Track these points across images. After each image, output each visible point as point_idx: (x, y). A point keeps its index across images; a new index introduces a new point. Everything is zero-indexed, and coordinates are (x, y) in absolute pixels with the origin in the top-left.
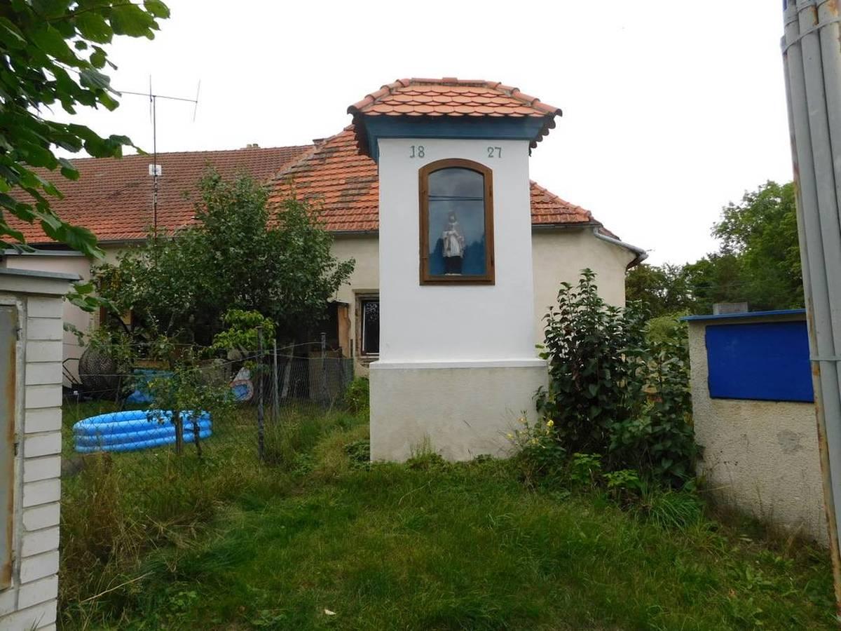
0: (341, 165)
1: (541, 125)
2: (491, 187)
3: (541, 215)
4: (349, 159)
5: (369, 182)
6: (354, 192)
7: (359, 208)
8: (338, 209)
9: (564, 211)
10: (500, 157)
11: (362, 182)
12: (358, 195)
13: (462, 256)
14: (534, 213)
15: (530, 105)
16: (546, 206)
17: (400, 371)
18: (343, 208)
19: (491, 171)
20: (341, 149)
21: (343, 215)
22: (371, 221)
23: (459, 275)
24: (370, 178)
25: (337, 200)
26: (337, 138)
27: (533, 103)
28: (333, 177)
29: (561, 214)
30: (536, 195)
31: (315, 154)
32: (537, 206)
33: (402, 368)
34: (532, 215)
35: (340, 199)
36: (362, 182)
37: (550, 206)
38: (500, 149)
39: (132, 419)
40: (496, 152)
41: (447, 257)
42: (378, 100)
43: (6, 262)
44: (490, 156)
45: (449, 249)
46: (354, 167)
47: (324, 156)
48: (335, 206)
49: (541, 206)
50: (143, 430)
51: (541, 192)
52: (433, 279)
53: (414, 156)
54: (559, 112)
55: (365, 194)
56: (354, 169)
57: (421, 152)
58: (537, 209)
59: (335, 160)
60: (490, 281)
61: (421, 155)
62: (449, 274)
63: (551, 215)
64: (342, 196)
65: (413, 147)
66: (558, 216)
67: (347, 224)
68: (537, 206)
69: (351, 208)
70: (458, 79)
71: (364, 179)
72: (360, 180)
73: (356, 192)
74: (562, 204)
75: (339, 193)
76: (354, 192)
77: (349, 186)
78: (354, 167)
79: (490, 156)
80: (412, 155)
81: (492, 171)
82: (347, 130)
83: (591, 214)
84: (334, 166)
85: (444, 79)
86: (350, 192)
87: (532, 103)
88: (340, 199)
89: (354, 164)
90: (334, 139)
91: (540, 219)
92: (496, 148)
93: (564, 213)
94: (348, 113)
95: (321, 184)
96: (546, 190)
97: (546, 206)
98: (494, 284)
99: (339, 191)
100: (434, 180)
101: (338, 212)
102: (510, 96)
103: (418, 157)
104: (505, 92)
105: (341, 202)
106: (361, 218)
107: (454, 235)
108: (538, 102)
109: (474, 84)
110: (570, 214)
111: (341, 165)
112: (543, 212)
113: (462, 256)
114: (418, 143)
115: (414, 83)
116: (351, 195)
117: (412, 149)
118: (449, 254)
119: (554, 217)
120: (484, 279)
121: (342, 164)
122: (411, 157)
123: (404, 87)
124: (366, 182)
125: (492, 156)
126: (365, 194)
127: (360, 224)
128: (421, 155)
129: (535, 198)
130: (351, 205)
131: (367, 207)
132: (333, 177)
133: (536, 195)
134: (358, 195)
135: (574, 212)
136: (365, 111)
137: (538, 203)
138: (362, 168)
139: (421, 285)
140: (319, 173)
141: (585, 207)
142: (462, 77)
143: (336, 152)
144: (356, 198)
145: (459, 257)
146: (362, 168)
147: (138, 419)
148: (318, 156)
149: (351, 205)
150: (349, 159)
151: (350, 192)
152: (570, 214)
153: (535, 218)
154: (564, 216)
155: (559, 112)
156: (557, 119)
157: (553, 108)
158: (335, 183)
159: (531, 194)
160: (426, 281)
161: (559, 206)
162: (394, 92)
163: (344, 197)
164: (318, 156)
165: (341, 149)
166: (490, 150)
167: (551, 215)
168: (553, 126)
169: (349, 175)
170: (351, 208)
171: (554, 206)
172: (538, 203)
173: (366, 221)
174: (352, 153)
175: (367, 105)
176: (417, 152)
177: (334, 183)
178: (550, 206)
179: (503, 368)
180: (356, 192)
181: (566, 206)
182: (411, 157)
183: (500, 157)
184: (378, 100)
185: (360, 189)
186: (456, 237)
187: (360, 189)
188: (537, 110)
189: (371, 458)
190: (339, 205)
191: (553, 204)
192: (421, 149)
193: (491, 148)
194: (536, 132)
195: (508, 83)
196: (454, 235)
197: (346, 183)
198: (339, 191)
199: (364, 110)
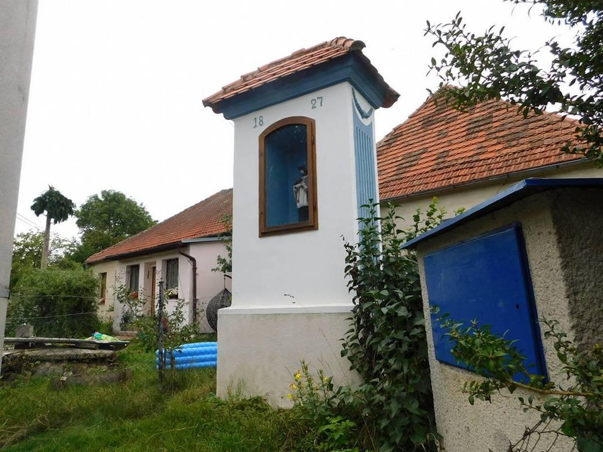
8: (392, 181)
12: (409, 166)
17: (239, 316)
18: (396, 180)
26: (402, 125)
31: (385, 142)
33: (239, 313)
36: (414, 156)
38: (322, 98)
39: (193, 347)
43: (189, 247)
44: (313, 108)
46: (411, 144)
47: (391, 141)
48: (390, 179)
50: (184, 356)
53: (256, 126)
56: (410, 147)
65: (255, 119)
69: (402, 179)
71: (417, 153)
72: (413, 154)
73: (408, 164)
78: (411, 144)
79: (313, 108)
80: (254, 126)
81: (315, 121)
86: (404, 165)
90: (400, 127)
92: (318, 98)
94: (205, 106)
95: (385, 163)
98: (318, 229)
101: (392, 183)
103: (260, 126)
105: (396, 175)
109: (316, 48)
114: (257, 114)
115: (271, 66)
122: (254, 127)
124: (417, 155)
130: (402, 176)
131: (414, 175)
134: (409, 166)
136: (211, 101)
139: (260, 237)
140: (385, 155)
142: (307, 46)
146: (416, 145)
147: (203, 347)
148: (386, 143)
149: (402, 176)
150: (408, 139)
151: (404, 165)
164: (386, 143)
166: (313, 102)
170: (402, 179)
176: (258, 121)
179: (319, 315)
182: (254, 127)
189: (217, 394)
190: (394, 178)
193: (313, 100)
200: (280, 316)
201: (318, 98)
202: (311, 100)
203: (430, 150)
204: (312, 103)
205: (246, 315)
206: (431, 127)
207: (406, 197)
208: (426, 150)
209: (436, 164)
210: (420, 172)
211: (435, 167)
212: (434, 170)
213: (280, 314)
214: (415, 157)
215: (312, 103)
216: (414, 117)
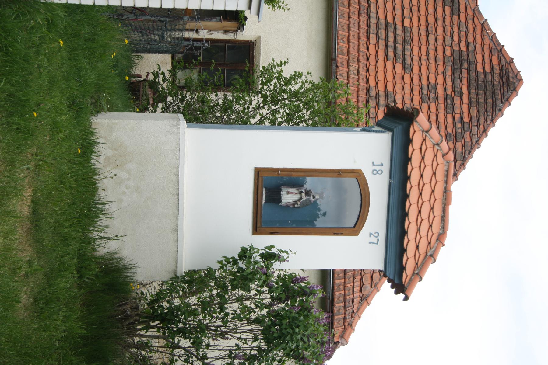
0: (431, 19)
1: (396, 281)
2: (342, 234)
3: (345, 283)
4: (440, 31)
5: (404, 60)
6: (391, 39)
7: (368, 49)
9: (349, 309)
10: (370, 243)
11: (404, 50)
12: (387, 46)
13: (282, 204)
14: (349, 274)
15: (416, 272)
16: (357, 289)
19: (357, 235)
20: (455, 17)
21: (359, 27)
22: (348, 65)
23: (264, 201)
24: (408, 61)
25: (381, 16)
27: (418, 274)
28: (415, 9)
29: (345, 307)
30: (372, 277)
32: (358, 278)
34: (345, 271)
35: (382, 21)
36: (404, 50)
37: (357, 294)
38: (377, 244)
40: (374, 240)
41: (280, 190)
42: (427, 135)
44: (371, 234)
45: (288, 193)
48: (373, 15)
49: (357, 283)
51: (376, 285)
52: (260, 179)
53: (374, 165)
54: (406, 298)
55: (386, 55)
56: (423, 38)
57: (378, 172)
58: (354, 278)
59: (440, 10)
60: (256, 231)
61: (375, 172)
62: (264, 192)
63: (344, 295)
64: (387, 23)
65: (382, 165)
66: (343, 304)
67: (347, 34)
68: (358, 278)
70: (450, 206)
71: (407, 53)
72: (408, 47)
73: (391, 43)
74: (358, 309)
75: (390, 19)
76: (391, 39)
77: (399, 32)
79: (371, 234)
82: (483, 25)
83: (343, 344)
84: (431, 10)
85: (451, 192)
86: (391, 35)
87: (417, 274)
88: (382, 21)
89: (432, 38)
91: (339, 281)
92: (378, 240)
93: (346, 311)
96: (378, 290)
97: (357, 289)
99: (394, 19)
100: (351, 183)
101: (364, 18)
102: (429, 254)
104: (433, 250)
105: (377, 24)
106: (353, 52)
107: (301, 198)
108: (419, 279)
110: (345, 318)
111: (431, 19)
112: (349, 286)
113: (282, 204)
116: (387, 36)
117: (381, 164)
118: (283, 193)
119: (342, 299)
120: (258, 225)
121: (433, 20)
122: (373, 163)
123: (443, 156)
124: (404, 55)
125: (370, 236)
126: (386, 55)
127: (345, 51)
128: (375, 172)
129: (369, 276)
132: (415, 9)
133: (372, 277)
134: (387, 46)
135: (346, 324)
137: (361, 279)
138: (424, 48)
139: (255, 168)
141: (353, 338)
142: (452, 210)
143: (452, 10)
144: (382, 43)
145: (281, 202)
146: (424, 48)
150: (440, 31)
152: (345, 318)
153: (342, 275)
154: (342, 311)
155: (406, 298)
156: (402, 296)
157: (411, 294)
158: (406, 12)
159: (374, 271)
160: (258, 172)
161: (356, 306)
162: (437, 147)
163: (384, 26)
165: (455, 17)
166: (376, 235)
167: (344, 295)
168: (397, 293)
169: (415, 30)
170: (368, 38)
171: (356, 301)
172: (361, 279)
173: (349, 59)
174: (449, 34)
175: (420, 125)
176: (378, 168)
177: (405, 11)
178: (357, 294)
180: (391, 43)
181: (355, 315)
182: (373, 163)
183: (370, 243)
184: (427, 135)
185: (395, 48)
186: (299, 200)
187: (395, 48)
188: (411, 278)
190: (373, 21)
191: (359, 299)
192: (380, 172)
193: (378, 234)
194: (391, 277)
195: (443, 253)
196: (301, 198)
197: (404, 28)
198: (394, 19)
199: (415, 124)
200: (176, 186)
201: (378, 240)
202: (377, 232)
203: (407, 77)
204: (375, 233)
205: (179, 159)
206: (449, 73)
207: (333, 57)
208: (408, 71)
209: (377, 94)
210: (372, 68)
211: (373, 93)
212: (368, 91)
213: (178, 186)
214: (401, 53)
215: (375, 233)
216: (482, 31)
